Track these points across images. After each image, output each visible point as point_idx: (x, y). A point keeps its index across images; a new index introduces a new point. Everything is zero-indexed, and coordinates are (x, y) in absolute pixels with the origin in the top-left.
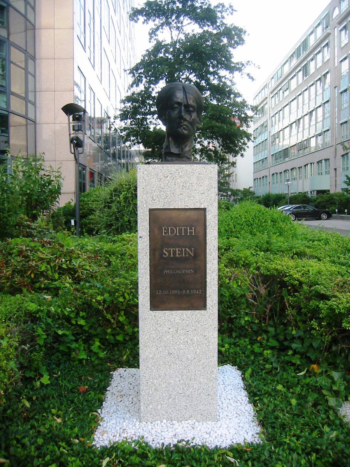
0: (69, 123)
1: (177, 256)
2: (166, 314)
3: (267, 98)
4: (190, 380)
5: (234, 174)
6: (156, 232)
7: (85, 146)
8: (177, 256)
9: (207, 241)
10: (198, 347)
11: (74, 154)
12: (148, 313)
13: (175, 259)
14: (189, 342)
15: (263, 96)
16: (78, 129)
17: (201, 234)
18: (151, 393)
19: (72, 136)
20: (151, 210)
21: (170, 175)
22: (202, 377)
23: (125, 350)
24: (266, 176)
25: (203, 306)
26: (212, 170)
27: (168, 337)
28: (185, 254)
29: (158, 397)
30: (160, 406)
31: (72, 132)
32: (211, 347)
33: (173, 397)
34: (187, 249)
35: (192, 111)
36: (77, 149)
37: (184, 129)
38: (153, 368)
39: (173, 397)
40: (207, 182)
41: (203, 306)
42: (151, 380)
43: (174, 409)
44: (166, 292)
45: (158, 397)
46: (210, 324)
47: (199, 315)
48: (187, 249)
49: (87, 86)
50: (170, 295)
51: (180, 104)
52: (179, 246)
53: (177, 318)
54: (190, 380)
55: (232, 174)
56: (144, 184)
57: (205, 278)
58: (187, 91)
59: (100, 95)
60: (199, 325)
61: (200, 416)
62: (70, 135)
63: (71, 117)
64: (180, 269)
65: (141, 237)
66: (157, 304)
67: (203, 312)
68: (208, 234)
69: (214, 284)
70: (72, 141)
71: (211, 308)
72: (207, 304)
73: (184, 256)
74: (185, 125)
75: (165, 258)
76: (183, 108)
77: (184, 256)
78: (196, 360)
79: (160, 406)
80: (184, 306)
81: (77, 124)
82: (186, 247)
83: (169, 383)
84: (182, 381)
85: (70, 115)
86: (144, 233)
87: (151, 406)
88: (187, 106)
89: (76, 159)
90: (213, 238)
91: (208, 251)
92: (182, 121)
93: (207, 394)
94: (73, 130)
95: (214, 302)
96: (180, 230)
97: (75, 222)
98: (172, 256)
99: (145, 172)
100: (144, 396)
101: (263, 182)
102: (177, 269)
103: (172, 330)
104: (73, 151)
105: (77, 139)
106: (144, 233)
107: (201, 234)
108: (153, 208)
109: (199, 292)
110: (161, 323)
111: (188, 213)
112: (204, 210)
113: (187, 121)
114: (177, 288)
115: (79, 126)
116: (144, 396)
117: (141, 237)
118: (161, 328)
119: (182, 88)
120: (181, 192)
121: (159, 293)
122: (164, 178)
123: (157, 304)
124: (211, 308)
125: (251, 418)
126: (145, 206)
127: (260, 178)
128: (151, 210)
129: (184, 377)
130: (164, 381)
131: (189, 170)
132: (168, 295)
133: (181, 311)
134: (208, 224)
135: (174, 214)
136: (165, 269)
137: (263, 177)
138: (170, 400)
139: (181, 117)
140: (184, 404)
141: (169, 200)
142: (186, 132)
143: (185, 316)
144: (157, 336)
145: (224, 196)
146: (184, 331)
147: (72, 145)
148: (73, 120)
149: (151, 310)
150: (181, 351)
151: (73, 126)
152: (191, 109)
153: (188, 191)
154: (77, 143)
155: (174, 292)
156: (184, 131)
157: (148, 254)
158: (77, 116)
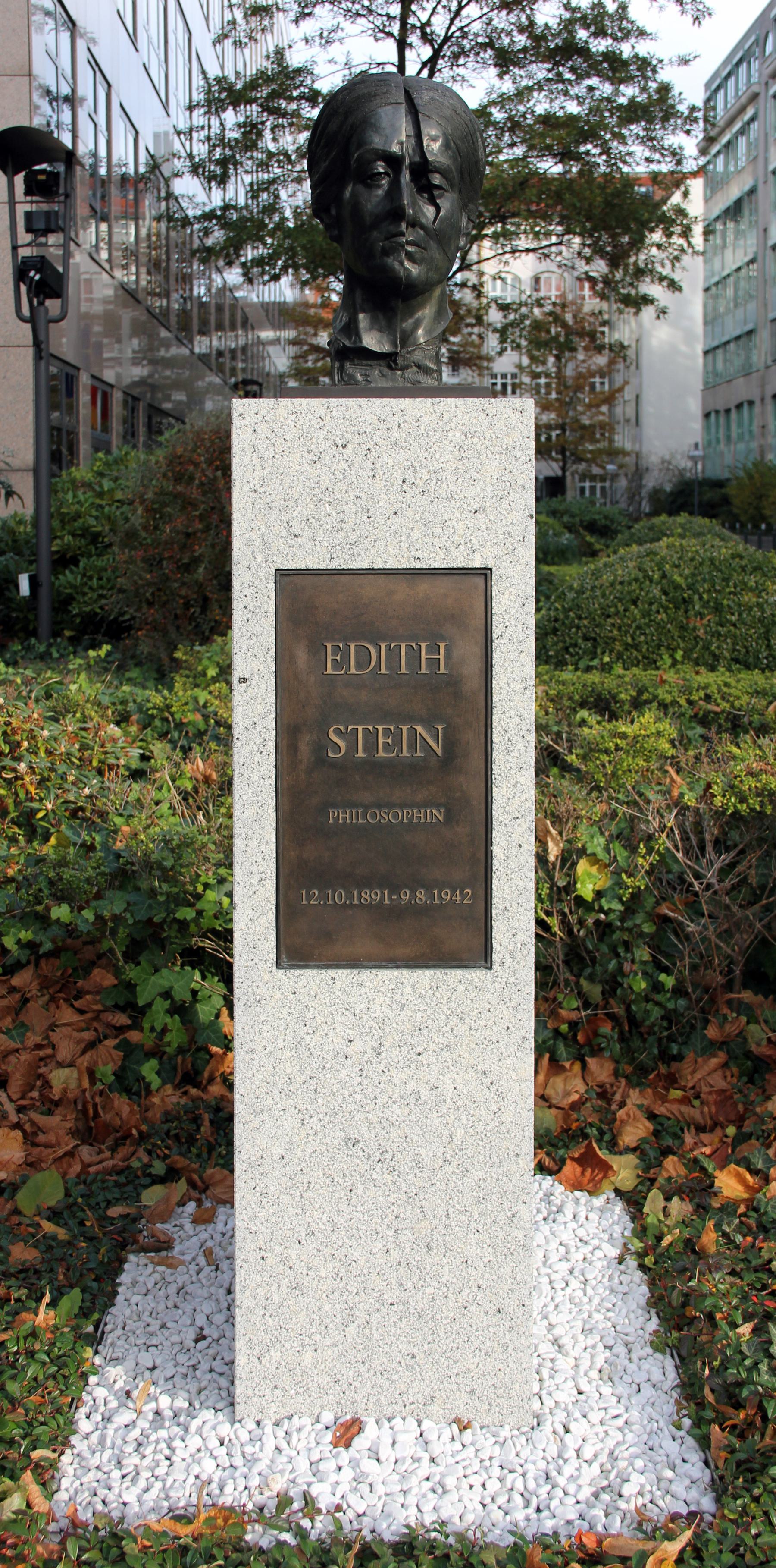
0: (12, 203)
1: (381, 753)
2: (338, 984)
3: (755, 97)
4: (429, 1248)
5: (628, 394)
6: (302, 656)
7: (71, 290)
8: (381, 753)
9: (495, 698)
10: (458, 1119)
11: (32, 320)
12: (266, 977)
13: (375, 769)
14: (425, 1094)
15: (742, 87)
16: (40, 225)
17: (472, 669)
18: (276, 1298)
19: (24, 252)
20: (281, 575)
21: (356, 440)
22: (473, 1238)
23: (160, 1142)
24: (751, 403)
25: (481, 955)
26: (514, 417)
27: (344, 1073)
28: (412, 746)
29: (302, 1316)
30: (309, 1354)
31: (24, 237)
32: (508, 1117)
33: (362, 1316)
34: (419, 729)
35: (439, 187)
36: (41, 303)
37: (410, 257)
38: (286, 1199)
39: (362, 1316)
40: (493, 467)
41: (481, 955)
42: (278, 1249)
43: (363, 1369)
44: (339, 896)
45: (302, 1316)
46: (502, 1025)
47: (461, 988)
48: (419, 729)
49: (82, 56)
50: (352, 906)
51: (394, 162)
52: (385, 716)
53: (380, 999)
54: (429, 1248)
55: (621, 389)
56: (259, 473)
57: (488, 841)
58: (420, 108)
59: (133, 91)
60: (462, 1029)
61: (465, 1397)
62: (15, 248)
63: (19, 179)
64: (390, 805)
65: (243, 680)
66: (299, 947)
67: (477, 975)
68: (497, 670)
69: (520, 868)
70: (21, 273)
71: (508, 961)
72: (495, 945)
73: (405, 753)
74: (409, 243)
75: (333, 765)
76: (406, 176)
77: (405, 753)
78: (449, 1169)
79: (309, 1354)
80: (400, 951)
81: (45, 207)
82: (411, 719)
83: (348, 1262)
84: (395, 1255)
85: (16, 173)
86: (255, 665)
87: (275, 1355)
88: (422, 169)
89: (37, 344)
90: (519, 686)
91: (496, 738)
92: (403, 226)
93: (492, 1309)
94: (29, 230)
95: (520, 937)
96: (394, 655)
97: (34, 582)
98: (361, 754)
99: (263, 429)
100: (252, 1311)
101: (740, 424)
102: (379, 807)
103: (357, 1046)
104: (26, 311)
105: (41, 263)
106: (255, 665)
107: (472, 669)
108: (291, 566)
109: (464, 896)
110: (320, 1019)
111: (424, 587)
112: (485, 573)
113: (423, 227)
114: (382, 878)
115: (47, 214)
116: (252, 1311)
117: (243, 680)
118: (317, 1038)
119: (402, 98)
120: (397, 507)
121: (312, 898)
122: (333, 451)
123: (299, 947)
124: (508, 961)
125: (670, 1408)
126: (260, 558)
127: (728, 411)
128: (281, 575)
129: (406, 1237)
130: (328, 1251)
131: (425, 420)
132: (345, 906)
133: (396, 973)
134: (497, 631)
135: (369, 589)
136: (334, 806)
137: (739, 406)
138: (352, 1329)
139: (396, 214)
140: (404, 1347)
141: (353, 537)
142: (414, 270)
143: (408, 990)
144: (302, 1071)
145: (593, 478)
146: (405, 1049)
147: (23, 288)
148: (27, 193)
149: (279, 966)
150: (394, 1132)
151: (28, 215)
152: (436, 179)
153: (423, 501)
154: (41, 282)
155: (370, 896)
156: (407, 264)
157: (271, 745)
158: (42, 177)
